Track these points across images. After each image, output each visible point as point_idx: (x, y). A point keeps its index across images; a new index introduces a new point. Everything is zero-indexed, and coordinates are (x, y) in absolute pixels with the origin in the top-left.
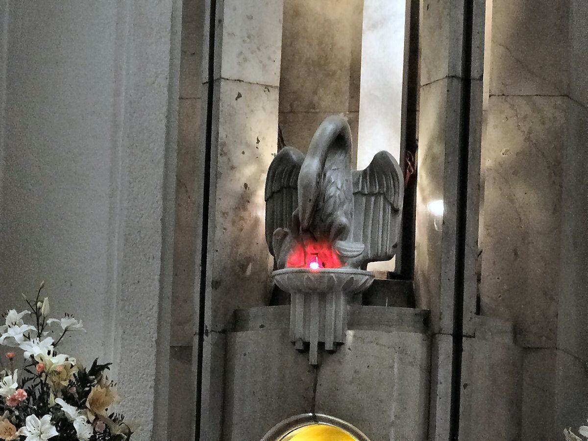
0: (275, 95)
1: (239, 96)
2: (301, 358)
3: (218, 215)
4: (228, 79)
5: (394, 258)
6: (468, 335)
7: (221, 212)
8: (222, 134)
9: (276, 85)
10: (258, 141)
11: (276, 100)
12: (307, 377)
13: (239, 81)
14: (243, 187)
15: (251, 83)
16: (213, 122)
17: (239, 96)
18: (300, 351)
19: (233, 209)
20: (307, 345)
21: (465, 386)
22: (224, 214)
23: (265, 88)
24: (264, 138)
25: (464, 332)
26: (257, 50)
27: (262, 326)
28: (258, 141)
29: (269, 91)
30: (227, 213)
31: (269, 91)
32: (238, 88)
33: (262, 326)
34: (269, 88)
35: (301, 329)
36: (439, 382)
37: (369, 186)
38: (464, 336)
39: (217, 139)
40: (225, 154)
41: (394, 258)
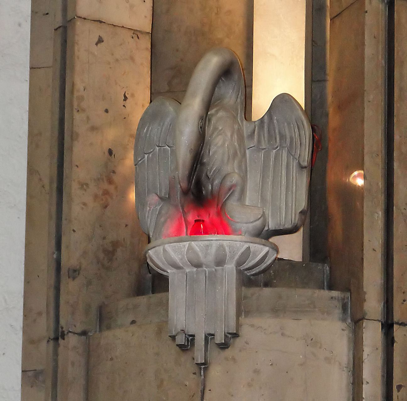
0: (146, 43)
1: (100, 40)
2: (185, 358)
3: (75, 186)
4: (85, 19)
5: (302, 230)
6: (400, 322)
7: (79, 183)
8: (79, 85)
9: (148, 31)
10: (126, 98)
11: (147, 49)
12: (191, 381)
13: (101, 22)
14: (107, 153)
15: (115, 26)
16: (68, 71)
17: (100, 40)
18: (182, 347)
19: (95, 180)
20: (191, 339)
21: (399, 387)
22: (82, 185)
23: (134, 34)
24: (133, 95)
25: (395, 319)
26: (245, 344)
27: (133, 322)
28: (126, 98)
29: (138, 38)
30: (87, 185)
31: (138, 38)
32: (96, 31)
33: (133, 322)
34: (138, 34)
35: (183, 318)
36: (364, 382)
37: (266, 139)
38: (305, 167)
39: (72, 92)
40: (84, 110)
41: (302, 230)
